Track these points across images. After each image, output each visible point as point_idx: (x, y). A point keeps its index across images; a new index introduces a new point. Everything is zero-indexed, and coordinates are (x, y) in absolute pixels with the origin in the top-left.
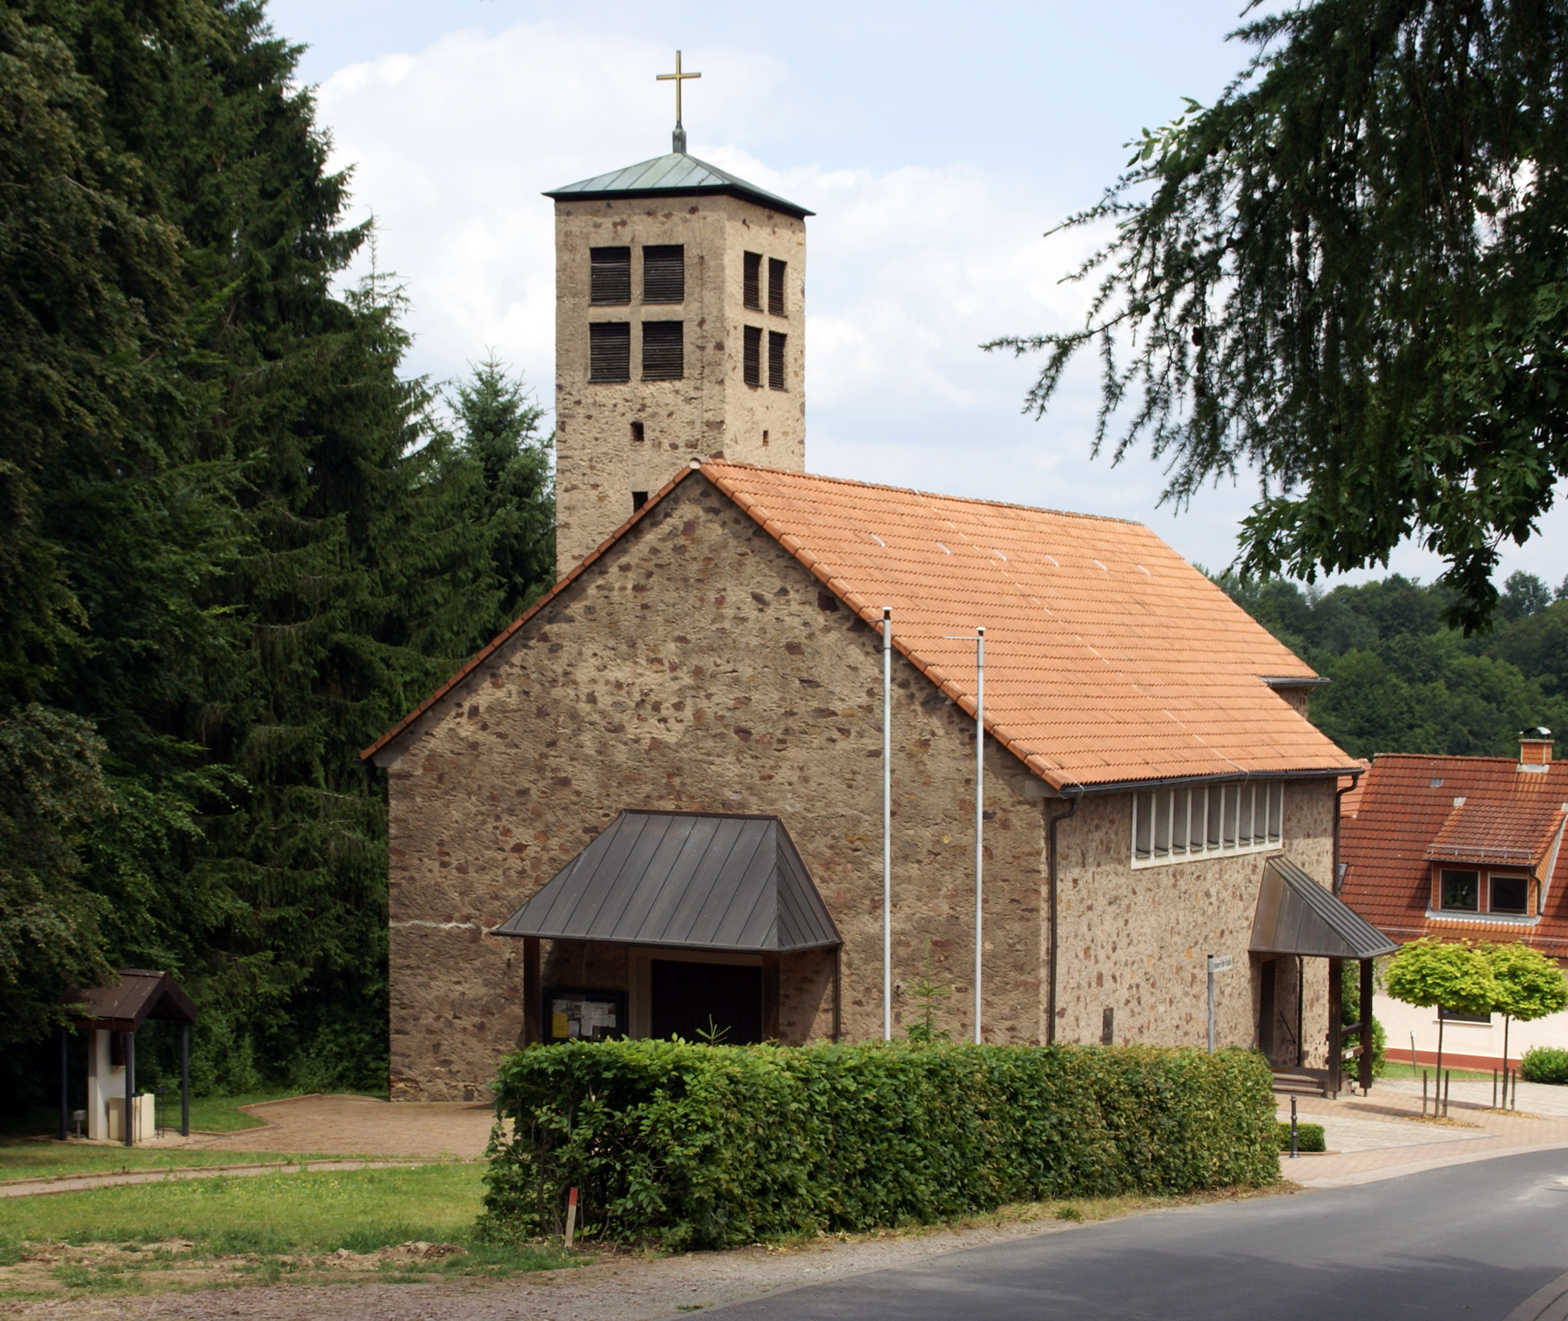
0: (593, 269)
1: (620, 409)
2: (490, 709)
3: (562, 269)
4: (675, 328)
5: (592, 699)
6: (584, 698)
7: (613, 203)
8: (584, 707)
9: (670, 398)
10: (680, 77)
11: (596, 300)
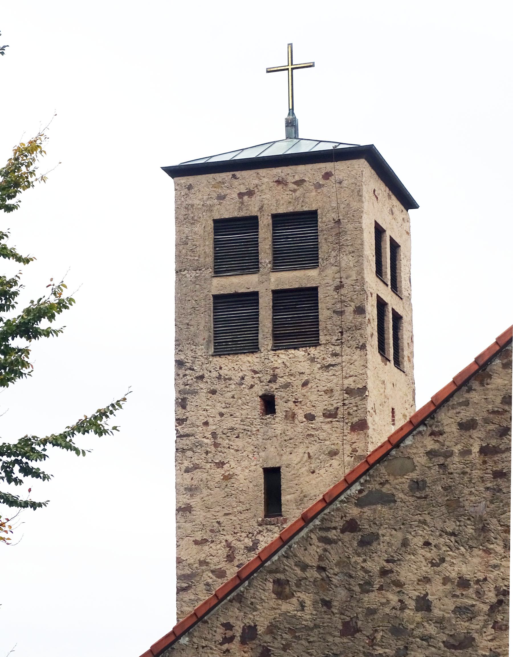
0: (216, 241)
1: (248, 381)
2: (272, 629)
3: (182, 243)
4: (310, 294)
5: (424, 604)
6: (412, 604)
7: (238, 174)
8: (411, 615)
9: (304, 366)
10: (291, 68)
11: (218, 272)
